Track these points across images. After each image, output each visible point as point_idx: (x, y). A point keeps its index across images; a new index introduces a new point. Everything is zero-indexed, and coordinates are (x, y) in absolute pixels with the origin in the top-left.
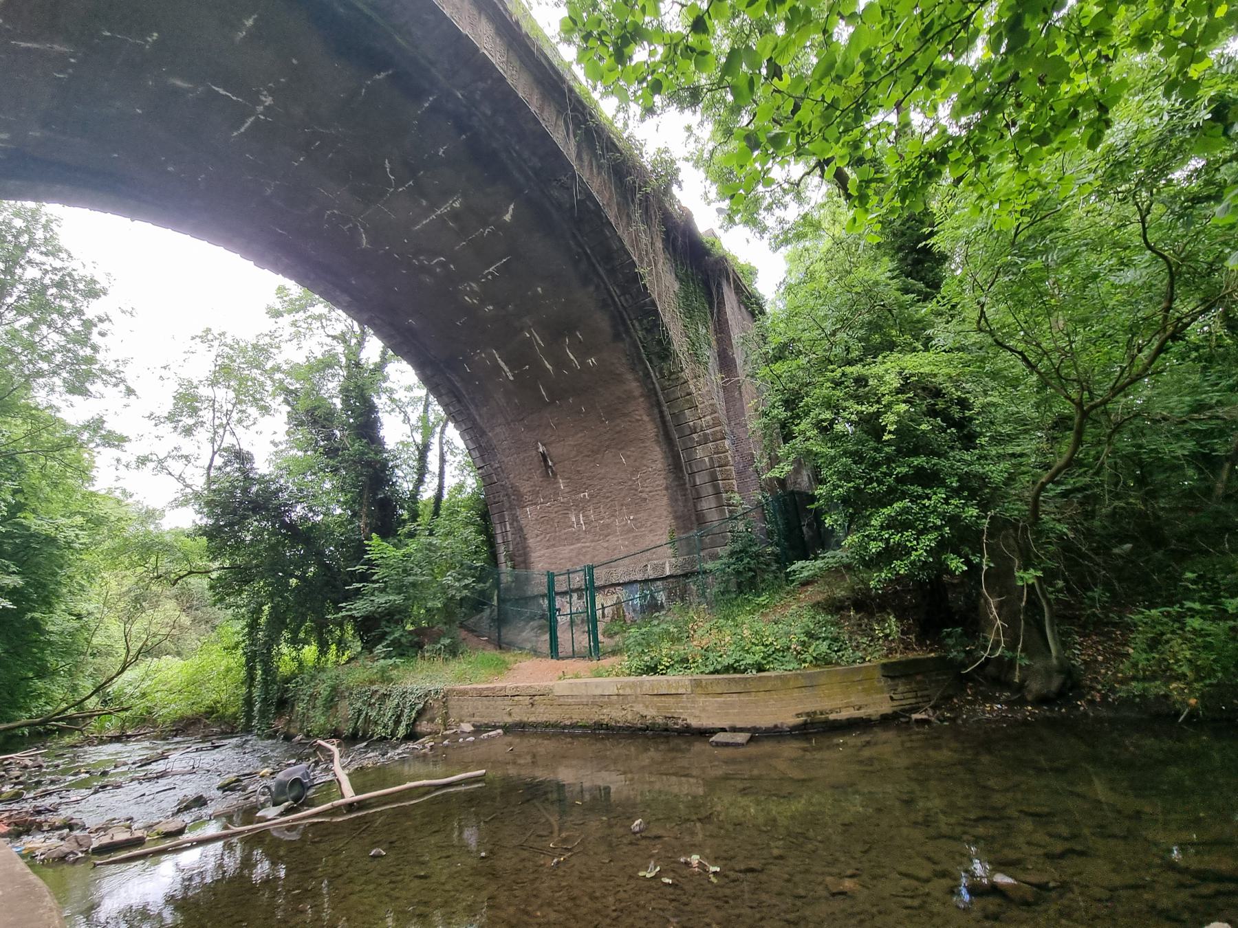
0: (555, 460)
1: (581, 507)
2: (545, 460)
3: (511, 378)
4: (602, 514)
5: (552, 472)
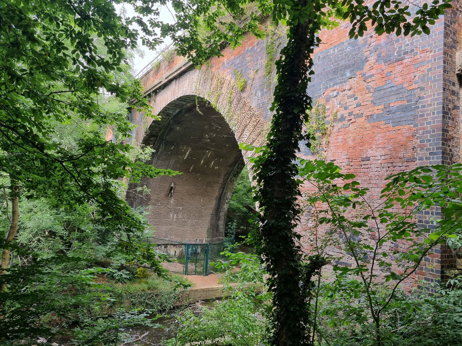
0: (175, 191)
1: (176, 212)
2: (171, 190)
3: (185, 158)
4: (185, 217)
5: (171, 195)
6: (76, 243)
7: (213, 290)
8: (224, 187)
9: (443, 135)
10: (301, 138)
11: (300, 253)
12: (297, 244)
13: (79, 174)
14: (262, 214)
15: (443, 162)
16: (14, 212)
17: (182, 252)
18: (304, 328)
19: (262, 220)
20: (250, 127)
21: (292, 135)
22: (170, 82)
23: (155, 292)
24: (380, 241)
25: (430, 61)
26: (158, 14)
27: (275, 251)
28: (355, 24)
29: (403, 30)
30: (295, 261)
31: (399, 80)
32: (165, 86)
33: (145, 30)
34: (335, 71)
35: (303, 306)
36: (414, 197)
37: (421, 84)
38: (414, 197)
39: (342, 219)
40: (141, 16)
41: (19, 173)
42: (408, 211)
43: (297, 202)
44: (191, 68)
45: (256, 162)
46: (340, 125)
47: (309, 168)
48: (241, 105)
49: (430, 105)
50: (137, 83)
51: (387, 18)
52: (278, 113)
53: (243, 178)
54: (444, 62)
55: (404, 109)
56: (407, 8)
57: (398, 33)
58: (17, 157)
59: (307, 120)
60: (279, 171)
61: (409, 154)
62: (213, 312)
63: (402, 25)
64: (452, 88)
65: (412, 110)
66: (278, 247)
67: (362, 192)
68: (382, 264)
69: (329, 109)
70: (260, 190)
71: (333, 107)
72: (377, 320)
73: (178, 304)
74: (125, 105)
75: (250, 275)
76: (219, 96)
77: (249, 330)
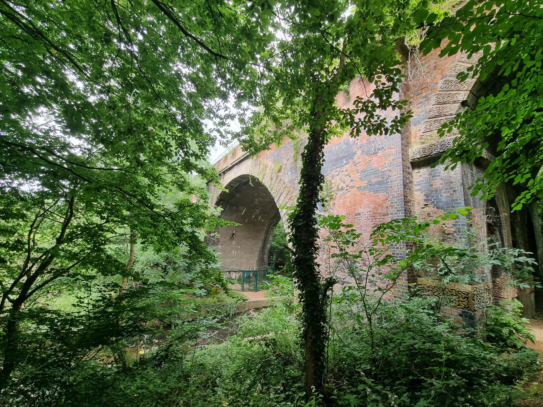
1: (237, 250)
6: (171, 272)
7: (258, 302)
8: (267, 233)
9: (404, 199)
10: (318, 201)
11: (319, 276)
12: (317, 270)
13: (175, 225)
14: (294, 250)
15: (405, 216)
16: (131, 251)
17: (240, 276)
18: (323, 327)
19: (294, 254)
20: (284, 195)
21: (312, 199)
22: (233, 166)
23: (223, 303)
24: (370, 267)
25: (393, 155)
26: (229, 126)
27: (303, 275)
28: (354, 129)
29: (384, 132)
30: (316, 282)
31: (376, 165)
32: (230, 169)
33: (221, 135)
34: (336, 160)
35: (322, 311)
36: (389, 238)
37: (389, 168)
38: (389, 238)
39: (347, 253)
40: (219, 127)
41: (136, 226)
42: (386, 248)
43: (316, 243)
44: (247, 158)
45: (289, 216)
46: (341, 192)
47: (325, 220)
48: (278, 181)
49: (396, 181)
50: (213, 169)
51: (373, 125)
52: (303, 185)
53: (279, 227)
54: (402, 155)
55: (380, 183)
56: (385, 119)
57: (381, 134)
58: (135, 215)
59: (322, 190)
60: (305, 222)
61: (384, 211)
62: (262, 317)
63: (383, 129)
64: (408, 170)
65: (384, 184)
66: (305, 272)
67: (358, 236)
68: (371, 282)
69: (333, 183)
70: (293, 235)
71: (336, 182)
72: (370, 319)
73: (238, 311)
74: (205, 181)
75: (286, 291)
76: (264, 175)
77: (285, 329)
